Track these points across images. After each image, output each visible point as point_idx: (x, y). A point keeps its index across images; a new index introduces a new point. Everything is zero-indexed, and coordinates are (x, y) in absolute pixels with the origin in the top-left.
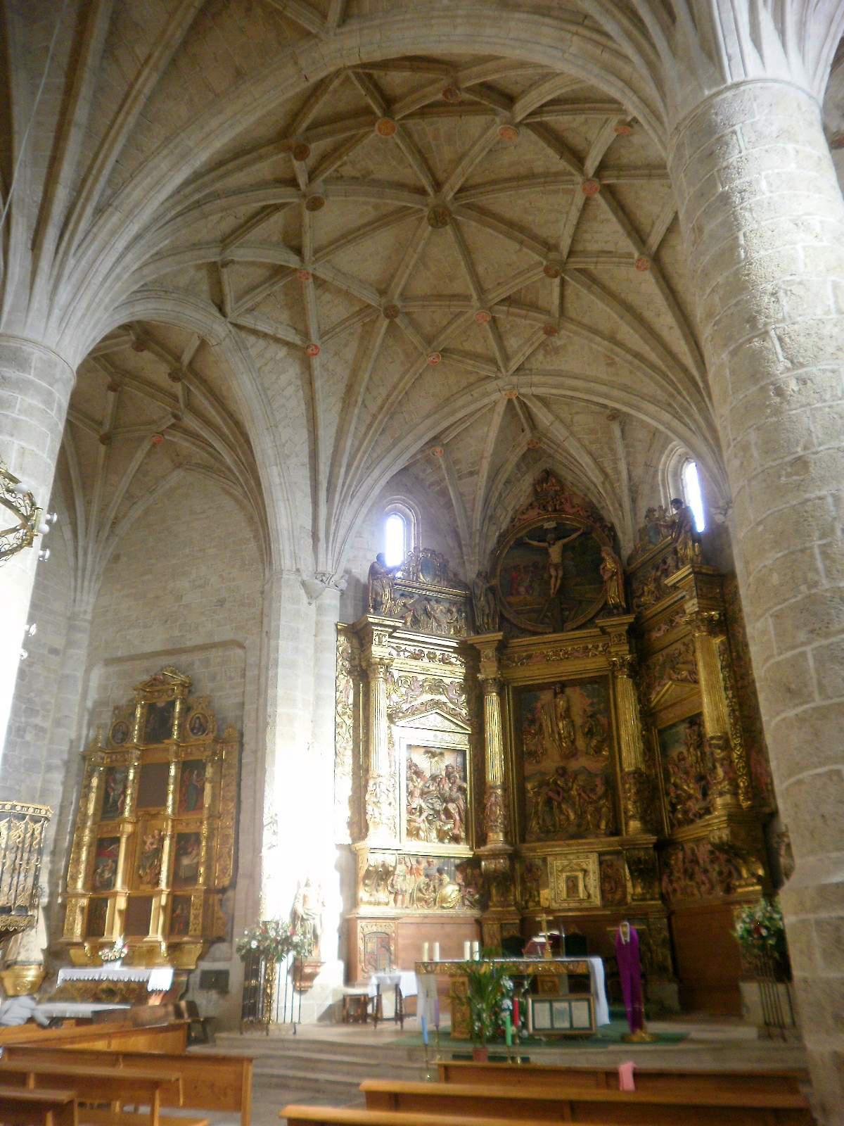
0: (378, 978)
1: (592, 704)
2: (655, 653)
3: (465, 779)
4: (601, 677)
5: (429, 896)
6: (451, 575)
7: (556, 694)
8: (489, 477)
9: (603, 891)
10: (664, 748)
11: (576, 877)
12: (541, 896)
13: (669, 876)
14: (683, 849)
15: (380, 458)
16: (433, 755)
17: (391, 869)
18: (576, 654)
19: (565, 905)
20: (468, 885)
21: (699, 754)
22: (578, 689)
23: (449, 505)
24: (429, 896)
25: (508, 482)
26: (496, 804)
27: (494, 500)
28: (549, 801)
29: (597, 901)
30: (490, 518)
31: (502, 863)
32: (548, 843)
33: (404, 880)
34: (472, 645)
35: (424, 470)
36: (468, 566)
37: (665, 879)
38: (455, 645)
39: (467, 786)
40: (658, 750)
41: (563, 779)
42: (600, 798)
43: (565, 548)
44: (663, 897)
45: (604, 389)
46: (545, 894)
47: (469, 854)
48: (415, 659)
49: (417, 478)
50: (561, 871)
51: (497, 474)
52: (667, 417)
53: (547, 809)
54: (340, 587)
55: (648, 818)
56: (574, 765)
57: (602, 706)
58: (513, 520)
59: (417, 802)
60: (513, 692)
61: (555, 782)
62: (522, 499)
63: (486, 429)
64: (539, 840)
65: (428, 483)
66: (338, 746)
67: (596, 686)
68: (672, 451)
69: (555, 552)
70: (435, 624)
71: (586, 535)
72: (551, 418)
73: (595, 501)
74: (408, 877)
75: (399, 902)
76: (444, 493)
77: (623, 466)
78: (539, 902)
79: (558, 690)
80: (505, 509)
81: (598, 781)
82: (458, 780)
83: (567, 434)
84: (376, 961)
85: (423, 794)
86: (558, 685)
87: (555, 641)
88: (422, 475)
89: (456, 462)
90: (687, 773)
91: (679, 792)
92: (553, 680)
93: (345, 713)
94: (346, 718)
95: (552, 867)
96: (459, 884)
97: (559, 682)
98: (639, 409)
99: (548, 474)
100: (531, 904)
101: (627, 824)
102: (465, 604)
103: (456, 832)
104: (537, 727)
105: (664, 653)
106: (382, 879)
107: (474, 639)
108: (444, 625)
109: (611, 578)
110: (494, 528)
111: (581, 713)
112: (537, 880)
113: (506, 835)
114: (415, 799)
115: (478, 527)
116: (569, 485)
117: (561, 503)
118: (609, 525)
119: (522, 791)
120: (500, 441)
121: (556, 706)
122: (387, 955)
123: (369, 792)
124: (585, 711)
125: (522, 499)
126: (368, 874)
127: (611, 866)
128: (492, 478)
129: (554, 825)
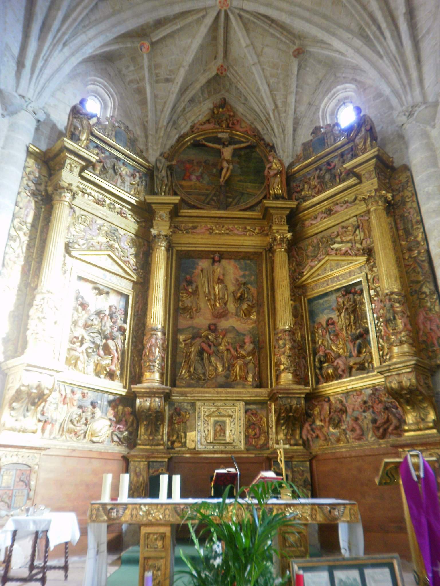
0: (16, 522)
1: (244, 276)
2: (305, 239)
3: (125, 322)
4: (255, 253)
5: (80, 428)
6: (139, 151)
7: (214, 262)
8: (180, 90)
9: (247, 437)
10: (312, 314)
11: (224, 422)
12: (188, 438)
13: (311, 425)
14: (329, 400)
15: (97, 22)
16: (100, 292)
17: (46, 392)
18: (236, 232)
19: (210, 447)
20: (118, 422)
21: (353, 318)
22: (232, 262)
23: (143, 102)
24: (80, 428)
25: (192, 101)
26: (156, 345)
27: (179, 109)
28: (201, 352)
29: (242, 446)
30: (174, 123)
31: (157, 402)
32: (198, 389)
33: (56, 408)
34: (149, 204)
35: (128, 67)
36: (150, 151)
37: (307, 426)
38: (134, 202)
39: (127, 327)
40: (306, 315)
41: (214, 335)
42: (249, 354)
43: (235, 154)
44: (306, 444)
45: (307, 14)
46: (192, 435)
47: (123, 392)
48: (97, 203)
49: (120, 72)
50: (209, 416)
51: (186, 90)
52: (358, 43)
53: (198, 358)
54: (37, 117)
55: (298, 373)
56: (224, 324)
57: (253, 277)
58: (192, 127)
59: (80, 332)
60: (177, 255)
61: (207, 337)
62: (200, 117)
63: (190, 41)
64: (189, 386)
65: (128, 79)
66: (7, 257)
67: (249, 262)
68: (334, 94)
69: (227, 152)
70: (120, 181)
71: (251, 148)
72: (248, 42)
73: (259, 128)
74: (61, 405)
75: (47, 432)
76: (141, 91)
77: (292, 99)
78: (185, 442)
79: (217, 258)
80: (186, 120)
81: (247, 340)
82: (119, 321)
83: (256, 61)
84: (10, 497)
85: (86, 326)
86: (217, 255)
87: (220, 218)
88: (124, 71)
89: (157, 66)
90: (337, 335)
91: (328, 351)
92: (212, 249)
93: (21, 229)
94: (21, 234)
95: (200, 412)
96: (110, 419)
97: (219, 252)
98: (334, 35)
99: (224, 104)
100: (176, 444)
101: (278, 377)
102: (146, 175)
103: (113, 368)
104: (194, 287)
105: (319, 236)
106: (33, 404)
107: (151, 199)
108: (127, 184)
109: (275, 175)
110: (175, 131)
111: (234, 282)
112: (185, 423)
113: (162, 375)
114: (78, 329)
115: (165, 124)
116: (240, 115)
117: (233, 124)
118: (271, 145)
119: (176, 342)
120: (197, 60)
121: (214, 271)
122: (26, 492)
123: (34, 307)
124: (237, 280)
125: (200, 117)
126: (18, 396)
127: (255, 414)
128: (183, 91)
129: (204, 374)
